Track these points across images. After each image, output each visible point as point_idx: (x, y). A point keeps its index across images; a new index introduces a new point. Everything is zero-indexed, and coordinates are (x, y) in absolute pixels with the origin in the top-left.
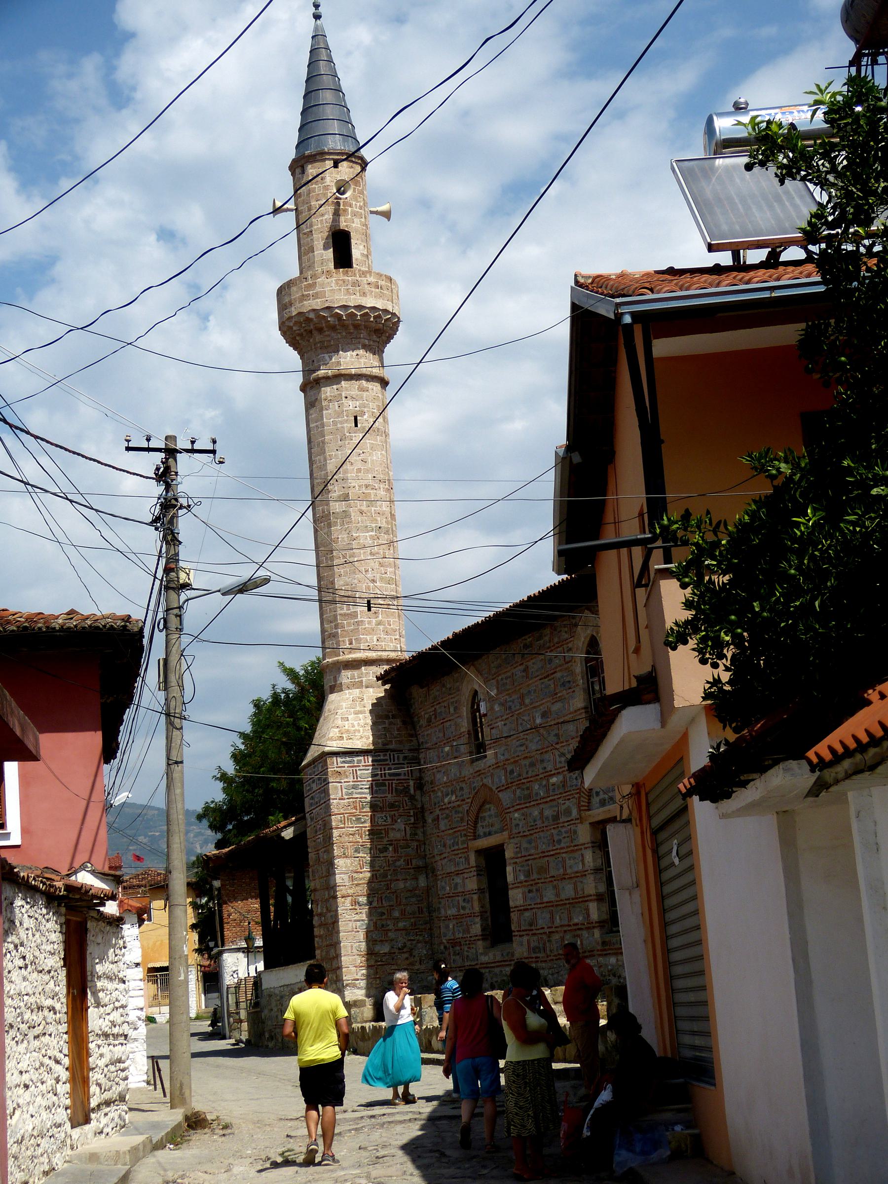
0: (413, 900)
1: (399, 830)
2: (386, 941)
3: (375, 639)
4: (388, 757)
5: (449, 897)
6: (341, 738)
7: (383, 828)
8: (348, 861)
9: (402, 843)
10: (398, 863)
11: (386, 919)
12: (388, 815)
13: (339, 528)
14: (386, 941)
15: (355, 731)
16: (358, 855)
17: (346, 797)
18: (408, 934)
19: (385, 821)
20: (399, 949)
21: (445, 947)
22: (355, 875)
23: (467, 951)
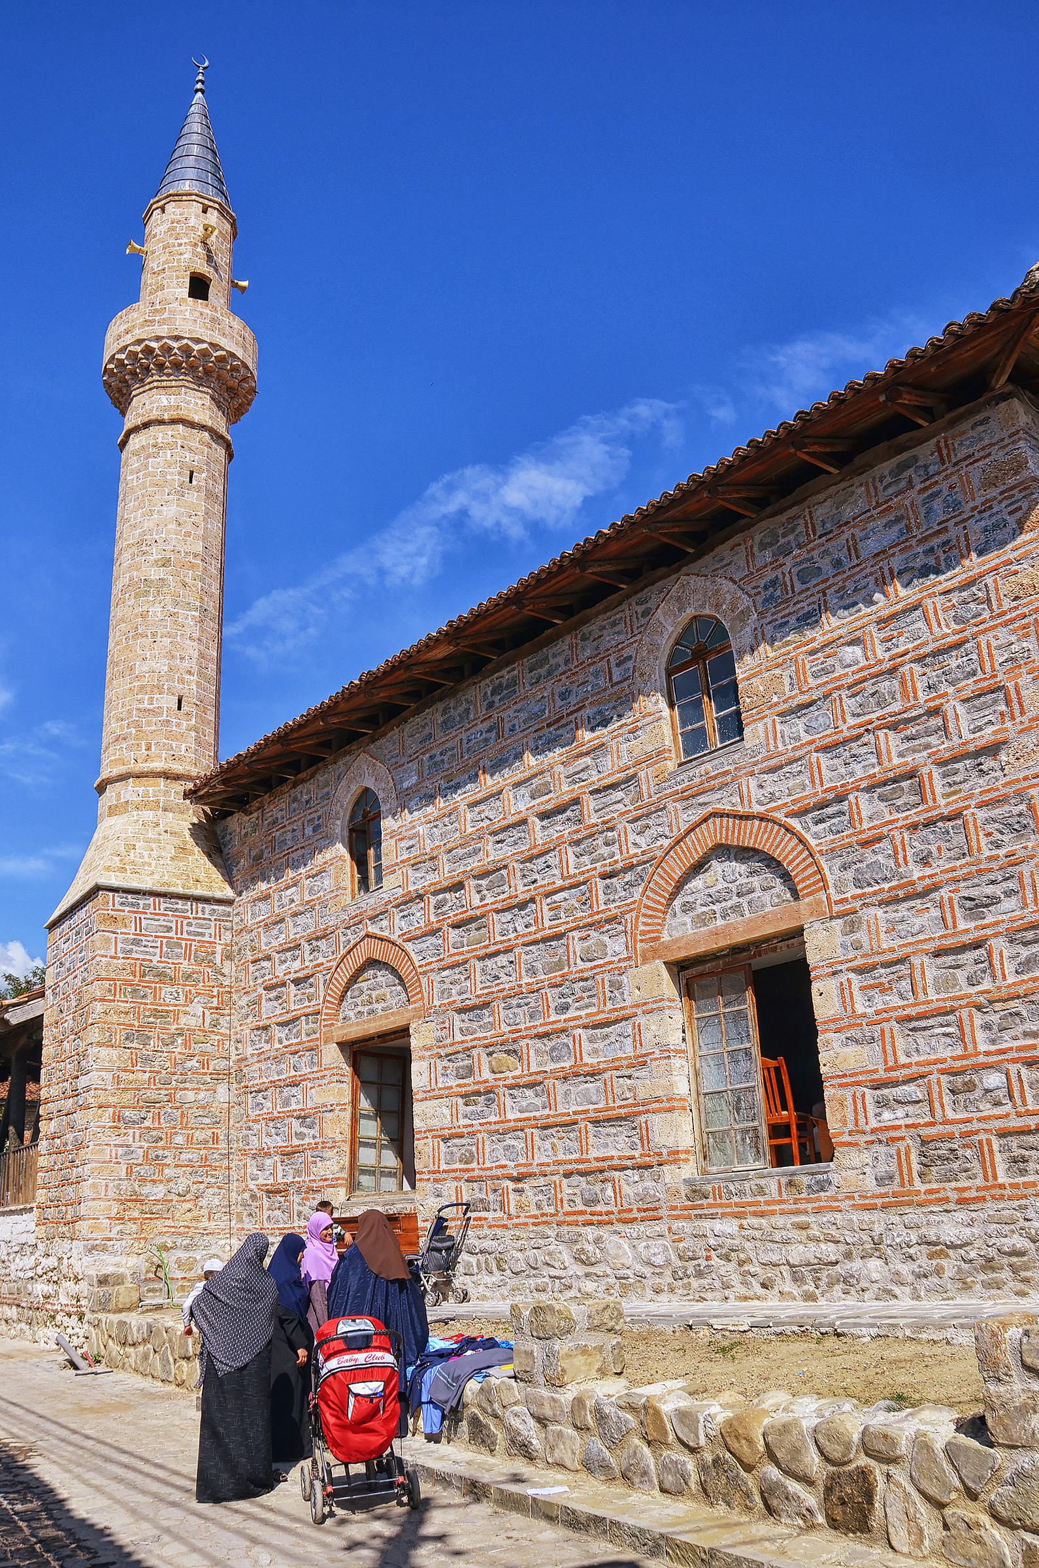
2: (161, 1181)
3: (183, 749)
6: (123, 870)
8: (114, 1053)
10: (189, 1064)
13: (151, 599)
14: (161, 1181)
15: (144, 864)
16: (131, 1045)
17: (122, 956)
20: (179, 1195)
22: (122, 1074)
23: (299, 1204)
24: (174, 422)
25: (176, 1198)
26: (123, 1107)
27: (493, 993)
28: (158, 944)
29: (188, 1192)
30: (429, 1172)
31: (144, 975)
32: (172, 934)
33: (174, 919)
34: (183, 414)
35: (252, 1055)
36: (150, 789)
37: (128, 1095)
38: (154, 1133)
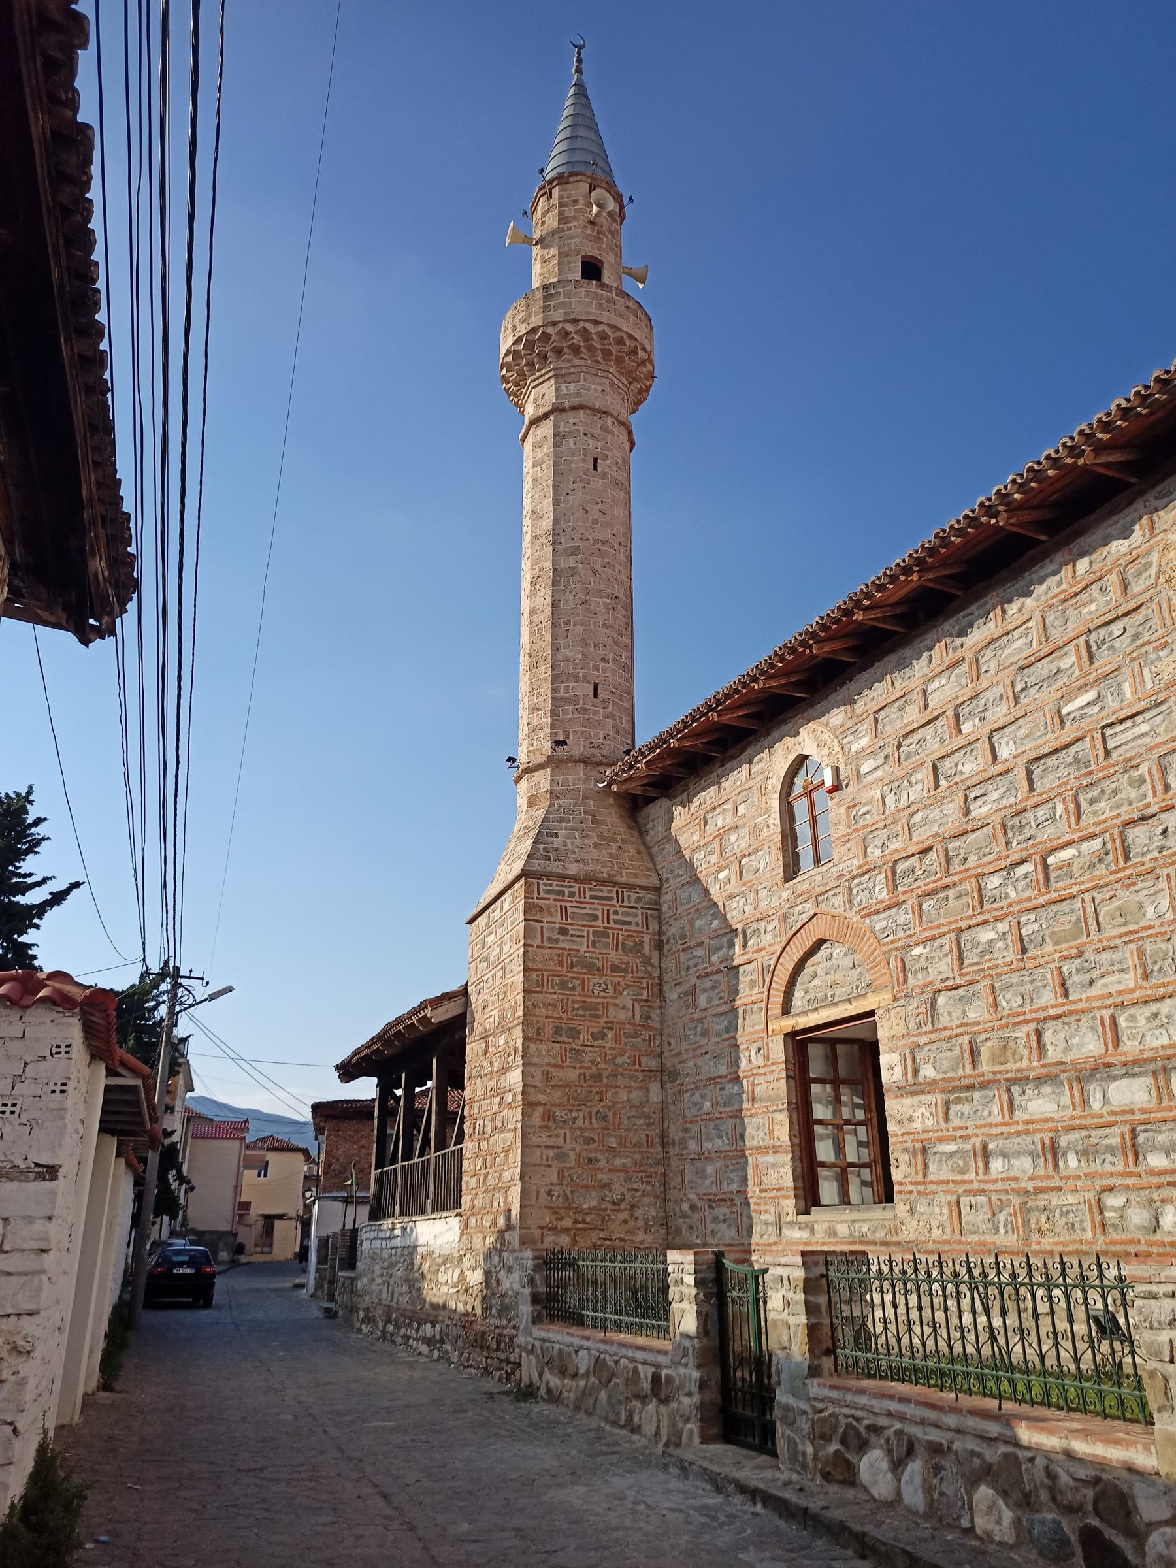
0: (640, 1122)
1: (624, 1008)
2: (594, 1187)
3: (601, 736)
4: (614, 895)
5: (710, 1120)
7: (600, 1000)
9: (629, 1028)
10: (619, 1060)
11: (596, 1151)
12: (609, 982)
15: (567, 851)
16: (559, 1039)
18: (628, 1179)
19: (604, 990)
20: (614, 1203)
21: (693, 1207)
22: (552, 1070)
24: (574, 408)
25: (610, 1207)
26: (553, 1105)
27: (983, 970)
28: (585, 934)
29: (623, 1200)
30: (911, 1183)
31: (572, 966)
32: (599, 923)
33: (600, 907)
34: (582, 400)
35: (687, 1050)
36: (570, 778)
37: (557, 1094)
38: (586, 1134)
